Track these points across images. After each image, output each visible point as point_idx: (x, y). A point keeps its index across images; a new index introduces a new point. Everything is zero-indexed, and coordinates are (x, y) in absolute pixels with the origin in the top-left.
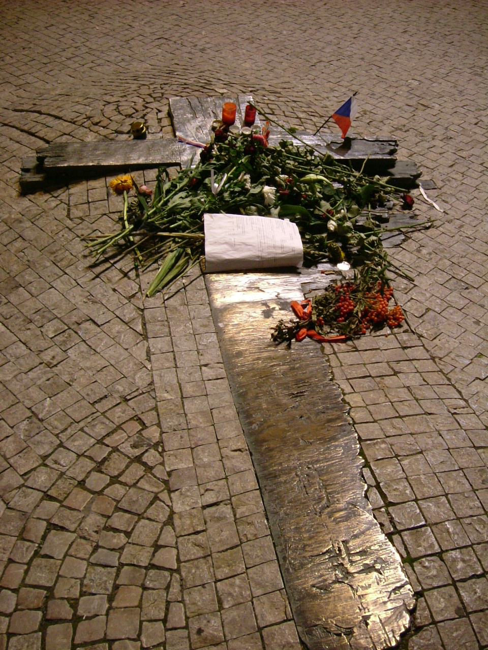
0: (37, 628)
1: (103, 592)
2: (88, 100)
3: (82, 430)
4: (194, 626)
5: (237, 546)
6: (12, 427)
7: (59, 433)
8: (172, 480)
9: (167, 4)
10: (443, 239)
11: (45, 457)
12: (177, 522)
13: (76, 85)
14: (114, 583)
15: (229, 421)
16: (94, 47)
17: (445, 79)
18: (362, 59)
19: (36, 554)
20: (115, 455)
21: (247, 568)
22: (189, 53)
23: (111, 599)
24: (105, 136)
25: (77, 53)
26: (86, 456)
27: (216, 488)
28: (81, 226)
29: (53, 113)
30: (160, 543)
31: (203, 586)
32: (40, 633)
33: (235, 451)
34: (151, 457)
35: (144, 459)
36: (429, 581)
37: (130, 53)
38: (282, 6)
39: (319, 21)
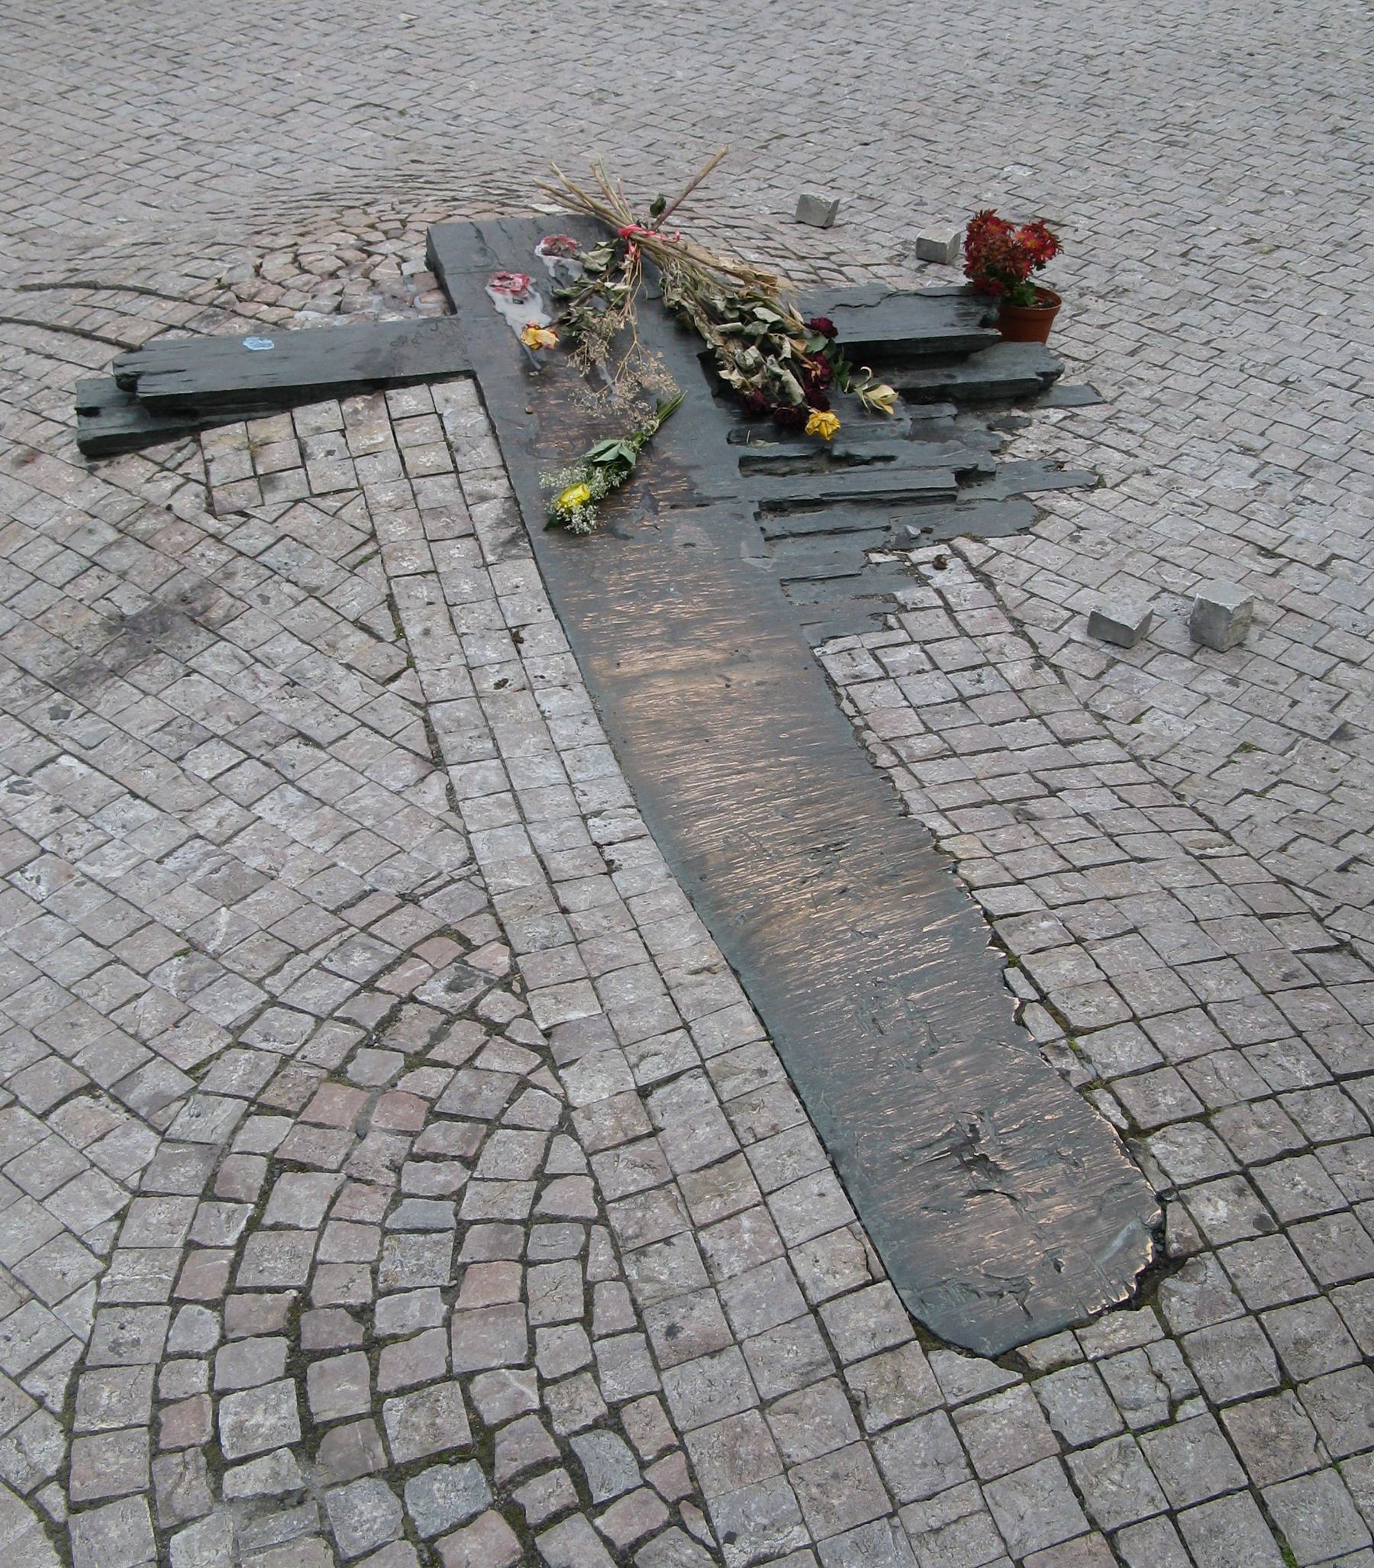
0: (280, 1371)
1: (431, 1282)
2: (216, 248)
3: (318, 965)
4: (657, 1326)
5: (735, 1154)
6: (145, 976)
7: (265, 977)
8: (556, 1045)
9: (365, 23)
10: (1128, 510)
11: (237, 1030)
12: (583, 1127)
13: (169, 223)
14: (454, 1261)
15: (671, 916)
16: (195, 134)
17: (1097, 157)
18: (883, 125)
19: (254, 1224)
20: (409, 1010)
21: (764, 1195)
22: (444, 134)
23: (449, 1293)
24: (275, 324)
25: (151, 151)
26: (337, 1019)
27: (664, 1048)
28: (244, 530)
29: (130, 283)
30: (549, 1170)
31: (667, 1241)
32: (292, 1381)
33: (696, 972)
34: (498, 1006)
35: (482, 1010)
36: (1188, 1169)
37: (291, 143)
38: (663, 12)
39: (763, 42)
